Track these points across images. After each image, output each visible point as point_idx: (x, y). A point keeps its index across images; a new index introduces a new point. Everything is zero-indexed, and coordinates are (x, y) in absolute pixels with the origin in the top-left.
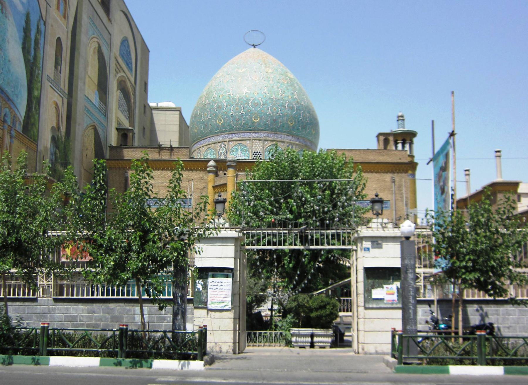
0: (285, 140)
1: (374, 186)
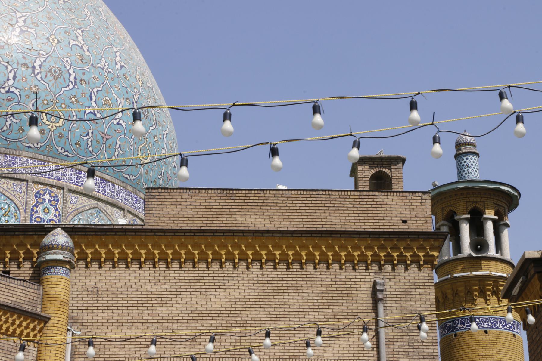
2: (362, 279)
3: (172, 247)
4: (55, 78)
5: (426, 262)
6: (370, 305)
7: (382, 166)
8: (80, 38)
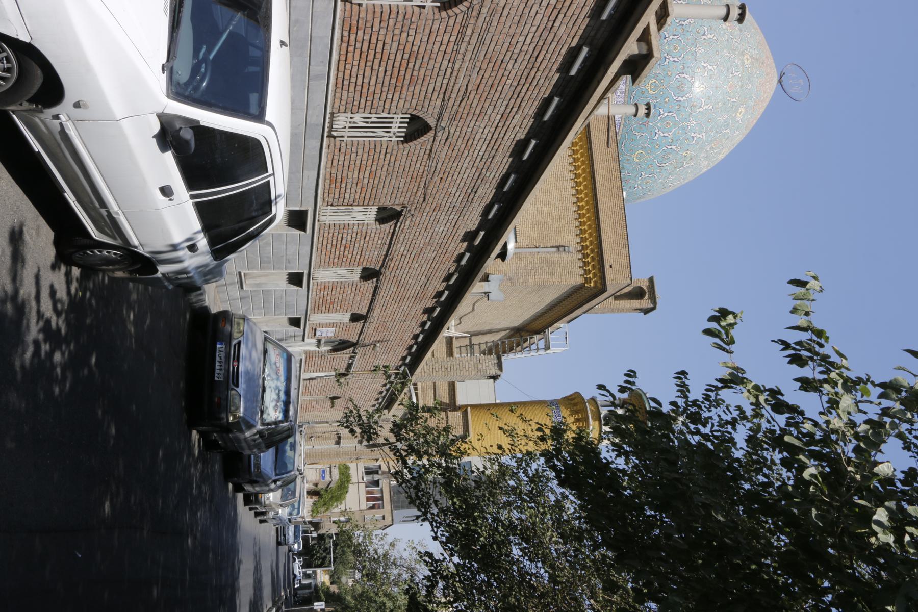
2: (571, 240)
3: (585, 189)
4: (678, 87)
5: (586, 279)
6: (555, 245)
7: (650, 294)
8: (707, 107)
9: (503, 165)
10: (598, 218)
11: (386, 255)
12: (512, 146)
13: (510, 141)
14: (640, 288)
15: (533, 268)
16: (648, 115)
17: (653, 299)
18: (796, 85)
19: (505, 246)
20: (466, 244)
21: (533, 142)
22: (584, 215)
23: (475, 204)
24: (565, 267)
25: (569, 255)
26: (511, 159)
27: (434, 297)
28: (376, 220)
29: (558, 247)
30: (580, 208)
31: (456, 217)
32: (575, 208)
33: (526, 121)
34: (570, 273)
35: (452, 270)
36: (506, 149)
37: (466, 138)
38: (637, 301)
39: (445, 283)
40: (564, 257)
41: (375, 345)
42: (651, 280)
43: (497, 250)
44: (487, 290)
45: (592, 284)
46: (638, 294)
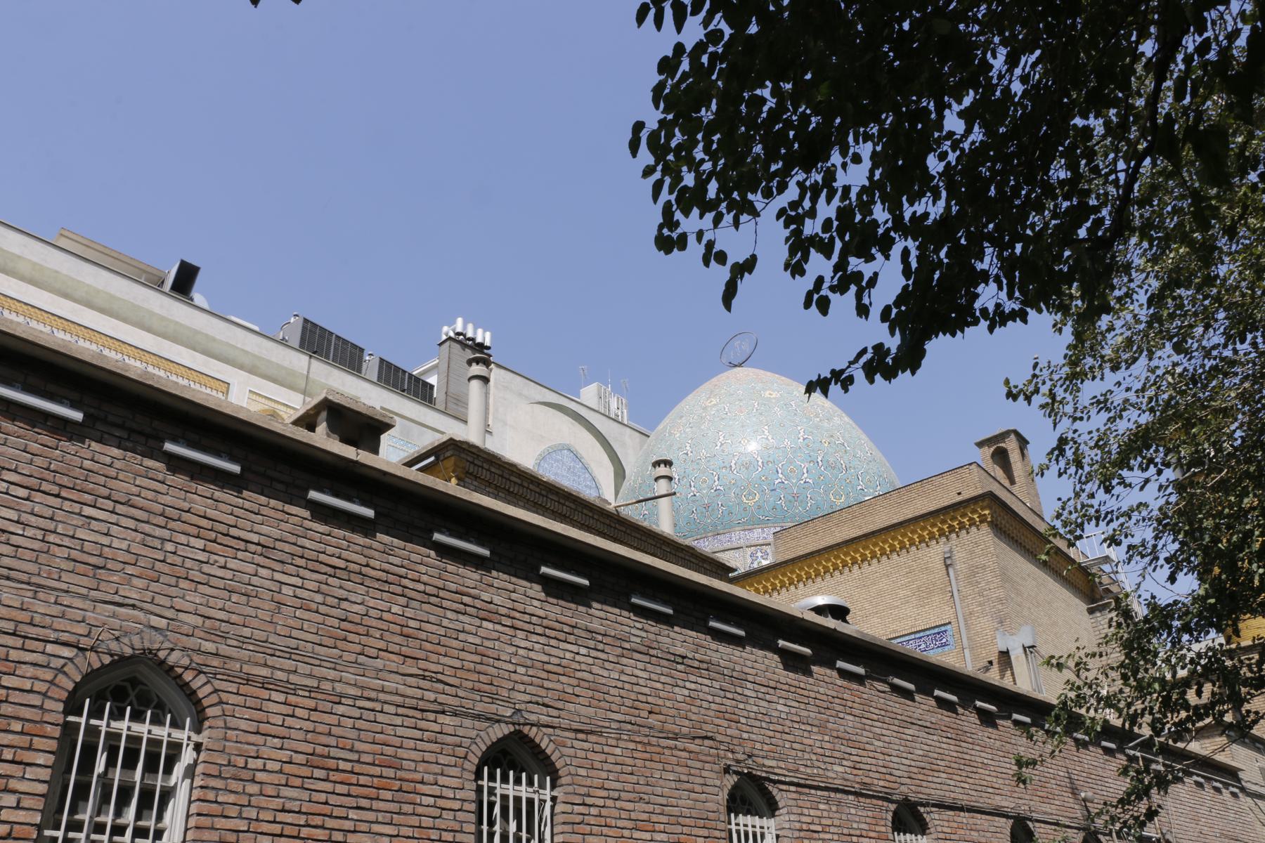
0: (742, 542)
1: (902, 593)
2: (936, 551)
5: (981, 522)
9: (613, 617)
10: (901, 524)
11: (856, 794)
12: (562, 603)
13: (548, 607)
14: (993, 456)
15: (981, 594)
16: (668, 463)
17: (1003, 436)
18: (742, 347)
19: (819, 610)
20: (815, 668)
21: (544, 570)
22: (901, 542)
23: (715, 658)
24: (972, 552)
25: (955, 550)
26: (595, 605)
27: (955, 712)
28: (773, 816)
29: (947, 566)
30: (893, 550)
31: (749, 685)
32: (895, 556)
33: (496, 583)
34: (979, 545)
35: (886, 688)
36: (569, 613)
37: (544, 675)
38: (1011, 456)
39: (917, 698)
40: (959, 555)
41: (1084, 800)
42: (980, 444)
43: (830, 622)
44: (1021, 650)
45: (987, 512)
46: (1001, 457)
